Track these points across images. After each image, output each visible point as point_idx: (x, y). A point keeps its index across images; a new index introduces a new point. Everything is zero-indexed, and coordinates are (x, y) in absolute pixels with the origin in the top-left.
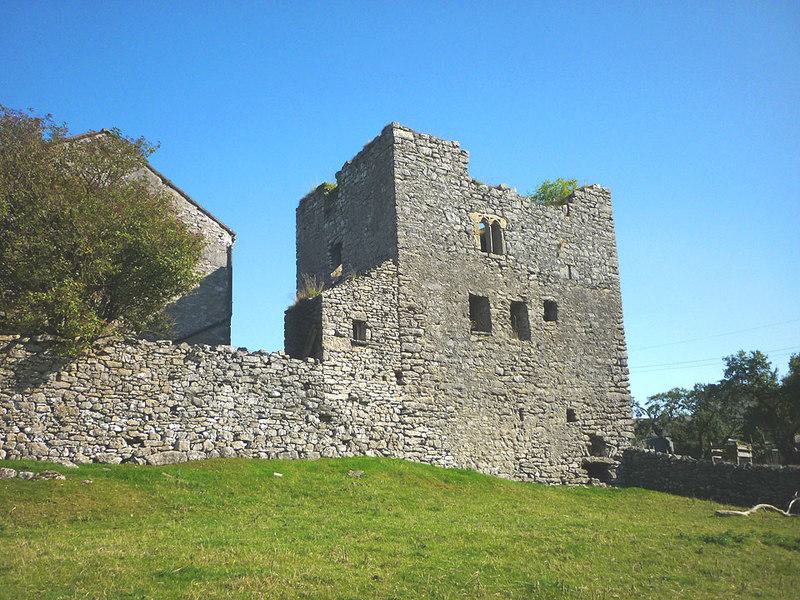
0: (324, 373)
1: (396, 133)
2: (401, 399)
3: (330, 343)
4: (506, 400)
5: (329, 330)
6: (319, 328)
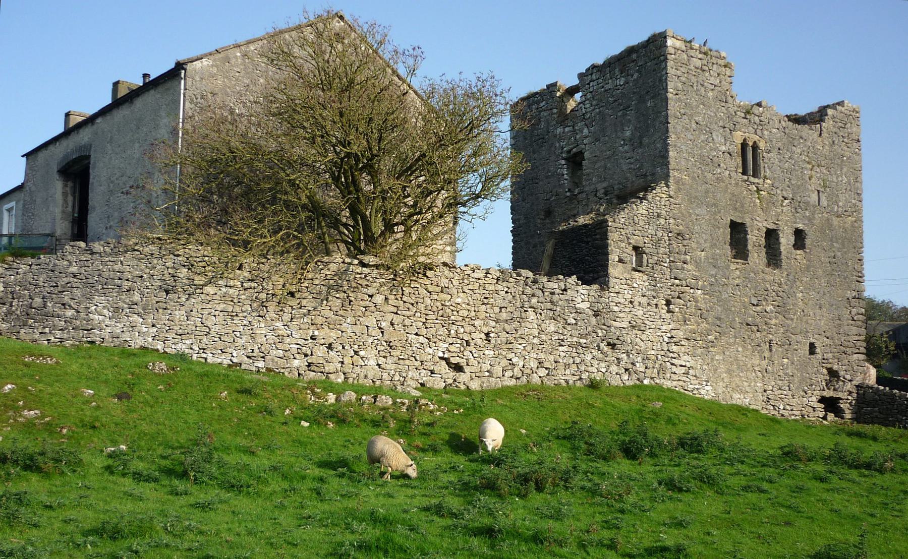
0: (610, 297)
1: (669, 42)
2: (671, 327)
3: (615, 271)
4: (758, 331)
5: (613, 258)
6: (607, 254)
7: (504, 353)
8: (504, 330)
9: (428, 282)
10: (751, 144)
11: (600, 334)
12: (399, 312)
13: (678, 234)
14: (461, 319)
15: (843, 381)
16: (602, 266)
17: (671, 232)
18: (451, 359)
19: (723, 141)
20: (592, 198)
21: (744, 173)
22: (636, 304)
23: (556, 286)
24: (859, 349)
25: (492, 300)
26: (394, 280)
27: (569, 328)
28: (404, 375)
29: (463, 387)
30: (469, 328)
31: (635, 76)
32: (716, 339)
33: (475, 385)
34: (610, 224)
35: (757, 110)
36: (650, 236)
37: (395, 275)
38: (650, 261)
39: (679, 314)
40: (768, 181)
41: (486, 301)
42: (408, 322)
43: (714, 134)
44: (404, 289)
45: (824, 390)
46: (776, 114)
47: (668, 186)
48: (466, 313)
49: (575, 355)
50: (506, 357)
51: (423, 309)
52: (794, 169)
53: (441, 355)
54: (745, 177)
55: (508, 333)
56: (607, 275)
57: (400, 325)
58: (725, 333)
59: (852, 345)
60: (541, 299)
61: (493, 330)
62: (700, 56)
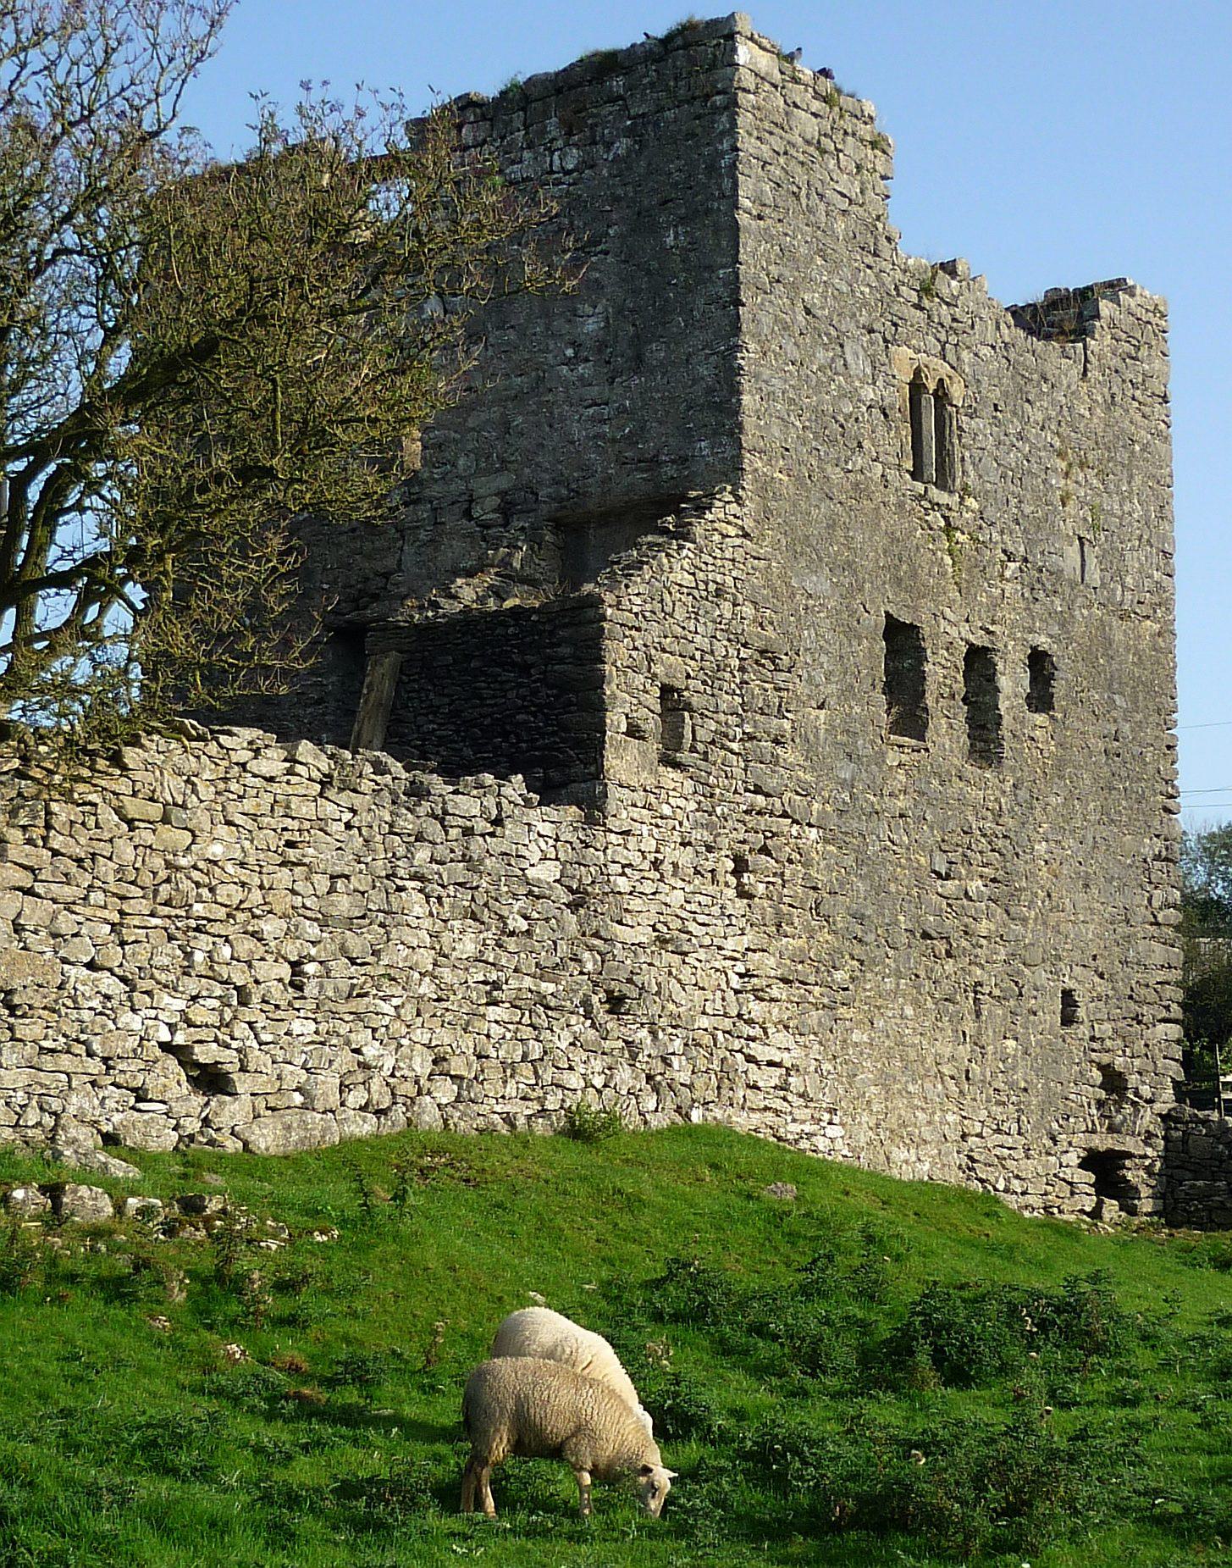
1: (744, 53)
2: (745, 941)
4: (949, 954)
5: (616, 720)
6: (597, 708)
7: (343, 1029)
8: (343, 949)
9: (123, 786)
10: (932, 386)
11: (589, 967)
12: (39, 888)
13: (762, 652)
14: (222, 913)
15: (1134, 1104)
16: (577, 744)
17: (745, 645)
18: (197, 1049)
19: (868, 371)
20: (451, 520)
21: (916, 474)
22: (667, 868)
23: (476, 811)
24: (1167, 1008)
25: (311, 851)
26: (20, 774)
27: (511, 944)
28: (56, 1105)
29: (232, 1145)
30: (246, 946)
31: (622, 146)
32: (853, 979)
33: (266, 1138)
34: (609, 611)
35: (947, 286)
36: (698, 655)
37: (25, 759)
38: (700, 733)
39: (766, 903)
40: (971, 502)
41: (292, 854)
42: (66, 923)
43: (847, 349)
44: (54, 807)
45: (1094, 1132)
46: (989, 303)
47: (739, 500)
48: (236, 894)
49: (527, 1033)
50: (348, 1043)
51: (111, 878)
52: (1029, 472)
53: (165, 1035)
54: (920, 487)
55: (353, 961)
56: (597, 773)
57: (43, 933)
58: (874, 962)
59: (1153, 997)
60: (442, 851)
61: (313, 951)
62: (817, 106)
